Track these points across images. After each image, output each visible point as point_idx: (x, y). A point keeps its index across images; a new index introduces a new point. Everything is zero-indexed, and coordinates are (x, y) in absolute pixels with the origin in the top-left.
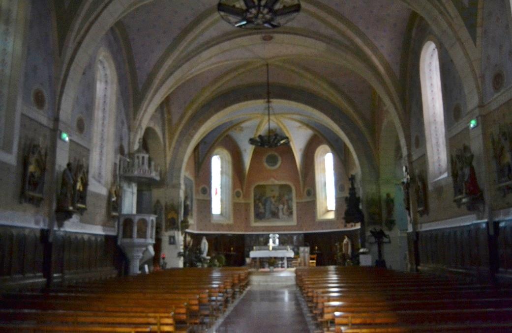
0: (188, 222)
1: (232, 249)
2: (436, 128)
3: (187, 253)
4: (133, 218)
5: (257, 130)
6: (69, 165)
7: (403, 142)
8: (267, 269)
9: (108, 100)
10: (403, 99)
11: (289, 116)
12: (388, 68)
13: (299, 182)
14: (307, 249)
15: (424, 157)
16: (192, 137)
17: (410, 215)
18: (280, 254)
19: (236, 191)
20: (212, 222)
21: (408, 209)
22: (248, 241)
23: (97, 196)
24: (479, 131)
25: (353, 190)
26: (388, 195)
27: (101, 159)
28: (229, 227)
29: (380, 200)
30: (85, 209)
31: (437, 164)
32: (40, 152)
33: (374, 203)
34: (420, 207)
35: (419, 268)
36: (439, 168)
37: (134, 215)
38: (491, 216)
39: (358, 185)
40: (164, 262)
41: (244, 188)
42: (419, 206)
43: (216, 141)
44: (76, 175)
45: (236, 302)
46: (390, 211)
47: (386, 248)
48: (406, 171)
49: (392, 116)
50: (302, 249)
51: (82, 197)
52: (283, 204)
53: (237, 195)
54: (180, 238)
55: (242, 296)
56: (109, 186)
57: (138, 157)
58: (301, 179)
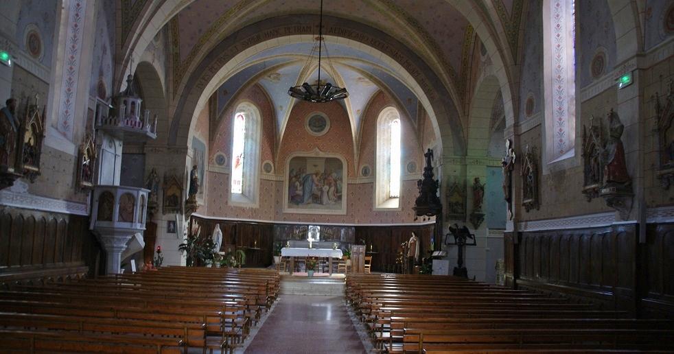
0: (195, 202)
2: (560, 87)
3: (193, 245)
4: (113, 191)
5: (300, 80)
6: (9, 102)
7: (508, 106)
8: (303, 273)
9: (82, 14)
10: (514, 45)
11: (343, 62)
14: (362, 249)
15: (539, 128)
16: (207, 81)
17: (510, 208)
18: (323, 253)
19: (265, 162)
20: (230, 204)
21: (509, 200)
22: (278, 231)
23: (60, 155)
24: (635, 91)
25: (429, 171)
26: (477, 180)
27: (68, 101)
28: (254, 212)
29: (465, 186)
30: (38, 173)
31: (557, 140)
32: (37, 115)
33: (457, 189)
34: (529, 198)
35: (518, 281)
37: (116, 187)
38: (644, 214)
39: (436, 163)
40: (159, 257)
41: (277, 159)
42: (525, 197)
43: (242, 90)
44: (23, 121)
45: (260, 324)
46: (478, 201)
47: (469, 252)
48: (510, 147)
49: (495, 69)
50: (355, 248)
51: (34, 154)
52: (330, 185)
53: (267, 168)
54: (184, 224)
55: (269, 314)
57: (125, 103)
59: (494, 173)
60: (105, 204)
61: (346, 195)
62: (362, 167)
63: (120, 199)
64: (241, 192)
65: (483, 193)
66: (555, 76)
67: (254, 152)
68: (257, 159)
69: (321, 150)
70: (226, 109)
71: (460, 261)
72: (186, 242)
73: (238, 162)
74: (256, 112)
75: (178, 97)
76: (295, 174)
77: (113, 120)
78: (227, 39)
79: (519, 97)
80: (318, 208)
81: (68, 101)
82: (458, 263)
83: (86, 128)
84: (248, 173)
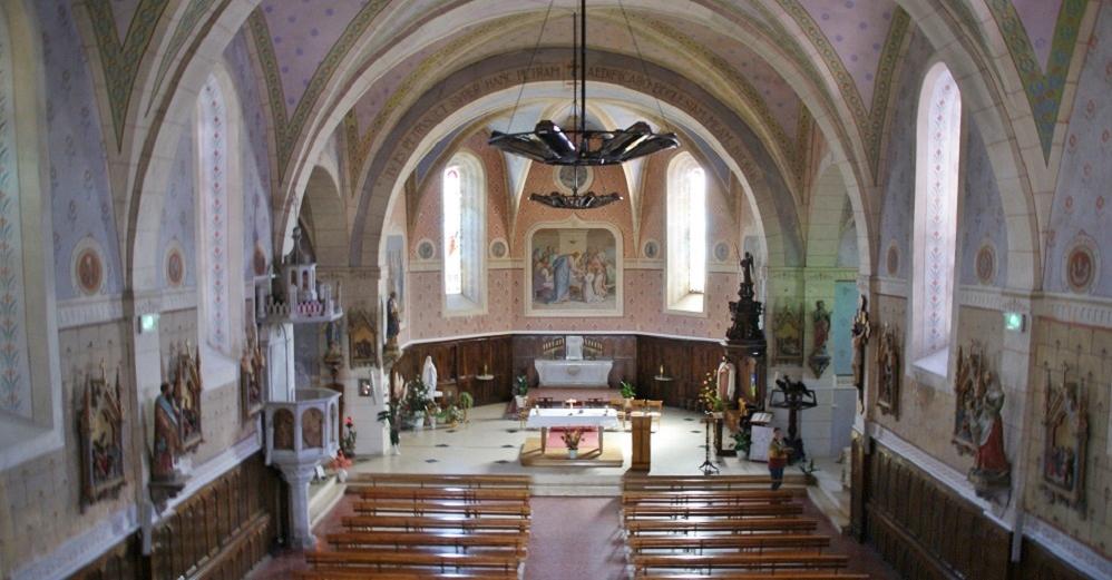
1: (486, 368)
2: (936, 250)
4: (291, 409)
10: (874, 158)
12: (847, 85)
13: (630, 223)
17: (861, 397)
19: (494, 241)
21: (860, 386)
25: (747, 286)
26: (819, 304)
27: (218, 299)
28: (481, 321)
29: (802, 314)
31: (928, 329)
33: (790, 318)
36: (933, 337)
40: (351, 432)
41: (513, 235)
46: (821, 338)
52: (596, 272)
53: (497, 251)
56: (241, 356)
58: (634, 219)
59: (846, 291)
60: (282, 426)
61: (621, 287)
62: (645, 244)
63: (303, 420)
64: (459, 291)
65: (829, 326)
66: (931, 231)
67: (476, 229)
68: (481, 238)
69: (582, 219)
70: (430, 175)
71: (793, 428)
72: (387, 408)
73: (452, 246)
74: (475, 164)
75: (359, 192)
76: (540, 255)
77: (281, 309)
78: (427, 94)
79: (879, 237)
80: (579, 308)
81: (218, 299)
82: (790, 431)
83: (247, 330)
84: (469, 262)
